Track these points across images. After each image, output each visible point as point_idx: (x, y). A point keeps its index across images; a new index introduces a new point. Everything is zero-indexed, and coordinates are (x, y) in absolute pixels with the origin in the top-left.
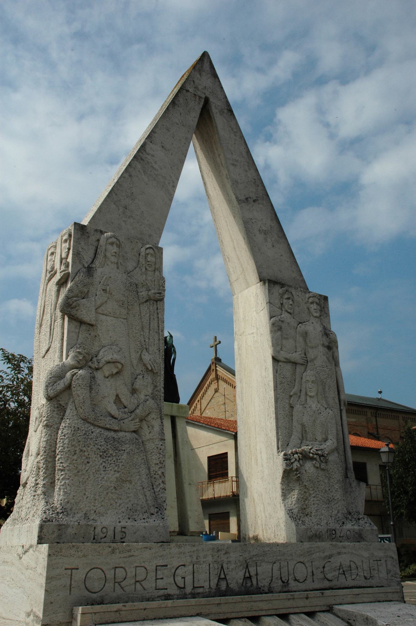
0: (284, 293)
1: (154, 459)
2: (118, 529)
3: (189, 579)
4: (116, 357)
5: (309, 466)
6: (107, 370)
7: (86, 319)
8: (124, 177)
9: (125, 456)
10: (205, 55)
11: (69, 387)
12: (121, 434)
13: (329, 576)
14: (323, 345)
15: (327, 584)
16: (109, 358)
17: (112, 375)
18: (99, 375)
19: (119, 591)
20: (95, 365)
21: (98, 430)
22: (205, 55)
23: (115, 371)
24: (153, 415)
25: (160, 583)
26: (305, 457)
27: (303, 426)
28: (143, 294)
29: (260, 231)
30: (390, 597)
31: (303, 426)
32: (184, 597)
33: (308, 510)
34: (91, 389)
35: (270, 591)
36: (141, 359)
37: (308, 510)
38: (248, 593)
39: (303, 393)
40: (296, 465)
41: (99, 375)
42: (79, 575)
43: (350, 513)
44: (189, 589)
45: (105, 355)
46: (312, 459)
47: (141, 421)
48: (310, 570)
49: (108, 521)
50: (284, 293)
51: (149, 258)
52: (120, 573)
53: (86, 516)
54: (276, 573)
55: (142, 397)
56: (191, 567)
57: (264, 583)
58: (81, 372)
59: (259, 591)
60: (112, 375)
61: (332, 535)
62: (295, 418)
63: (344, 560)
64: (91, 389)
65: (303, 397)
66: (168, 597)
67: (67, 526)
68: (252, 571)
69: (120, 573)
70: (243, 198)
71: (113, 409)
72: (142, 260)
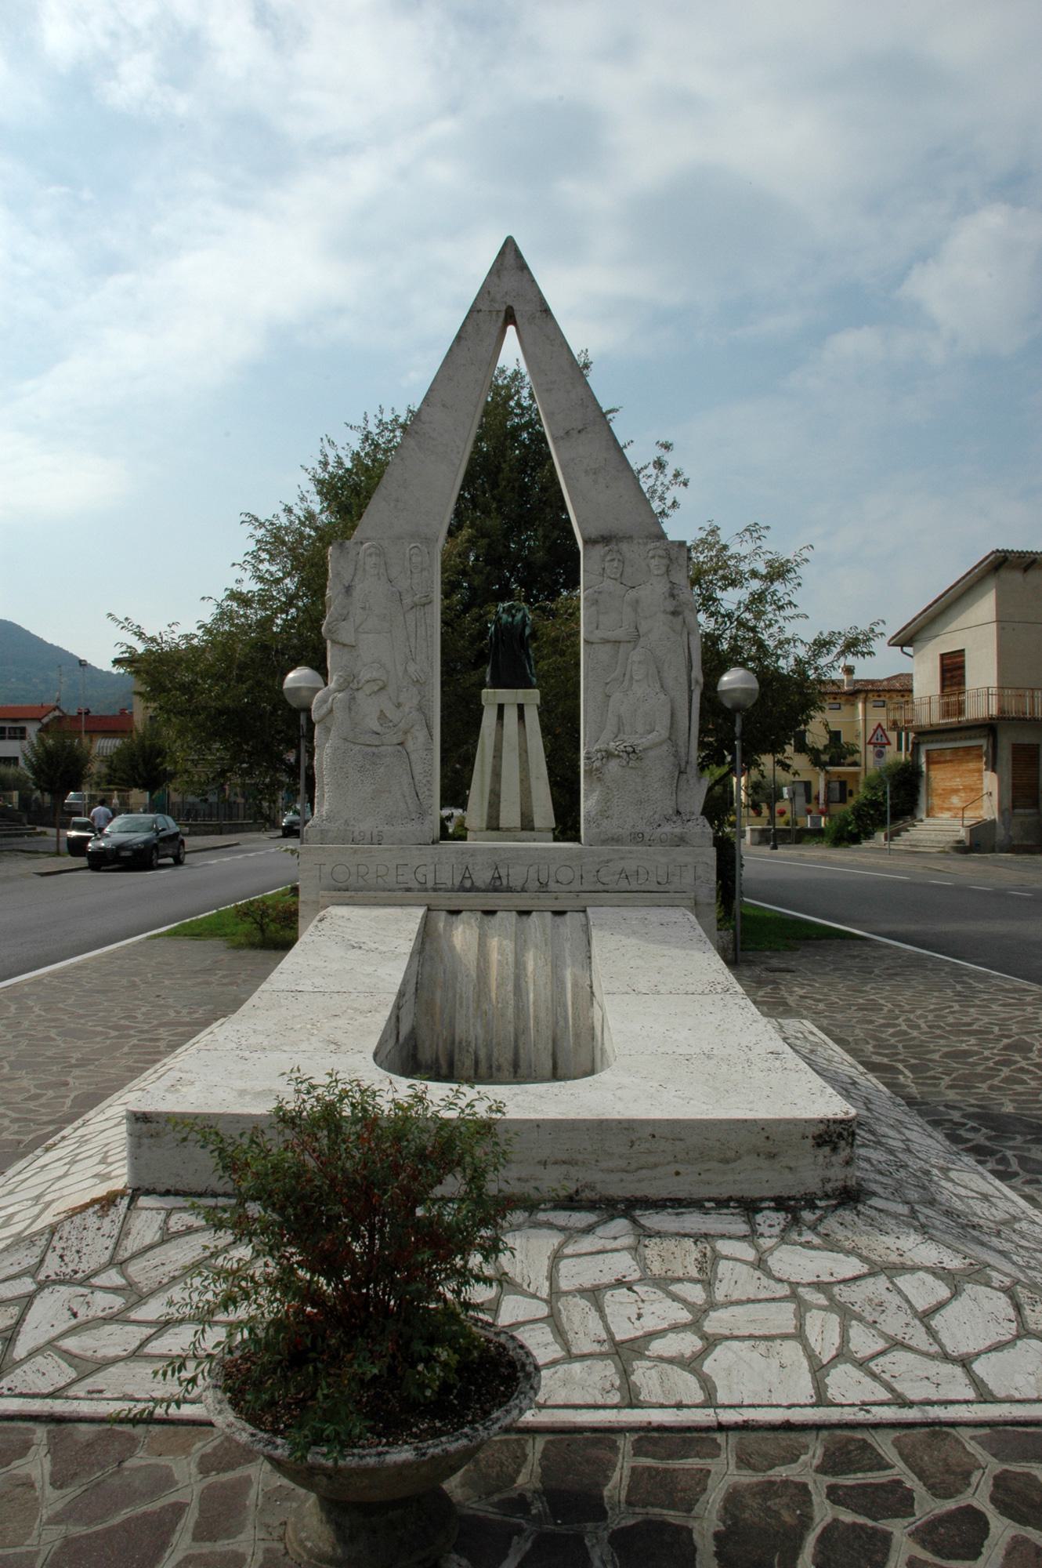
0: (605, 555)
1: (418, 769)
2: (375, 833)
3: (430, 877)
4: (375, 675)
5: (613, 765)
6: (367, 689)
7: (346, 642)
8: (479, 311)
9: (382, 770)
10: (510, 243)
11: (331, 711)
12: (382, 748)
13: (604, 880)
14: (665, 612)
15: (600, 887)
16: (367, 677)
17: (375, 693)
18: (360, 695)
19: (361, 882)
20: (355, 686)
21: (358, 747)
22: (510, 243)
23: (376, 688)
24: (417, 727)
25: (400, 879)
26: (609, 755)
27: (619, 717)
28: (408, 600)
29: (586, 472)
30: (677, 902)
31: (619, 717)
32: (426, 890)
33: (610, 813)
34: (350, 709)
35: (523, 890)
36: (406, 670)
37: (610, 813)
38: (496, 890)
39: (627, 677)
40: (597, 764)
41: (360, 695)
42: (327, 869)
43: (678, 813)
44: (430, 884)
45: (365, 675)
46: (619, 756)
47: (406, 733)
48: (578, 874)
49: (366, 826)
50: (605, 555)
51: (414, 559)
52: (363, 869)
53: (346, 823)
54: (533, 875)
55: (407, 710)
56: (432, 867)
57: (516, 883)
58: (340, 695)
59: (509, 890)
60: (375, 693)
61: (638, 838)
62: (610, 709)
63: (630, 865)
64: (350, 709)
65: (626, 683)
66: (408, 890)
67: (328, 831)
68: (503, 872)
69: (363, 869)
70: (561, 433)
71: (375, 725)
72: (407, 564)
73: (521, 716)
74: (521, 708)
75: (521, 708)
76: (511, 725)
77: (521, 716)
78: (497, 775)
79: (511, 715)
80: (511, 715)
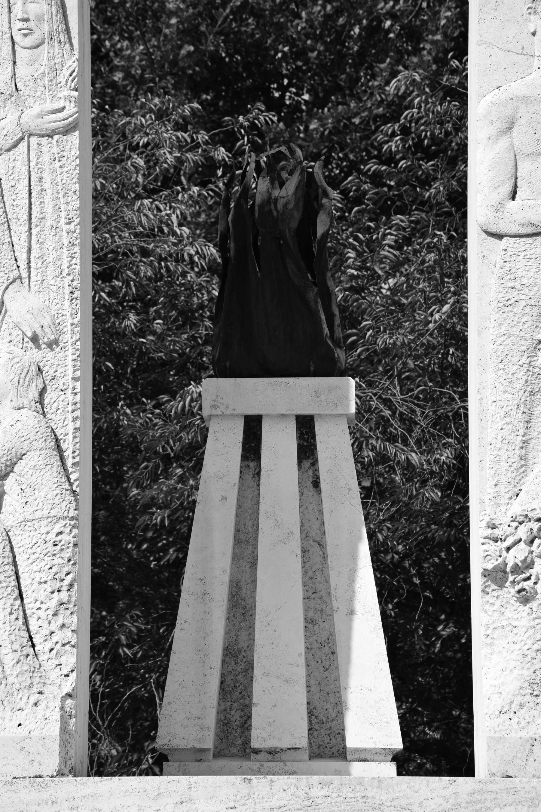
73: (307, 450)
74: (306, 426)
75: (306, 426)
76: (281, 476)
77: (307, 450)
78: (241, 607)
79: (279, 444)
80: (279, 444)
